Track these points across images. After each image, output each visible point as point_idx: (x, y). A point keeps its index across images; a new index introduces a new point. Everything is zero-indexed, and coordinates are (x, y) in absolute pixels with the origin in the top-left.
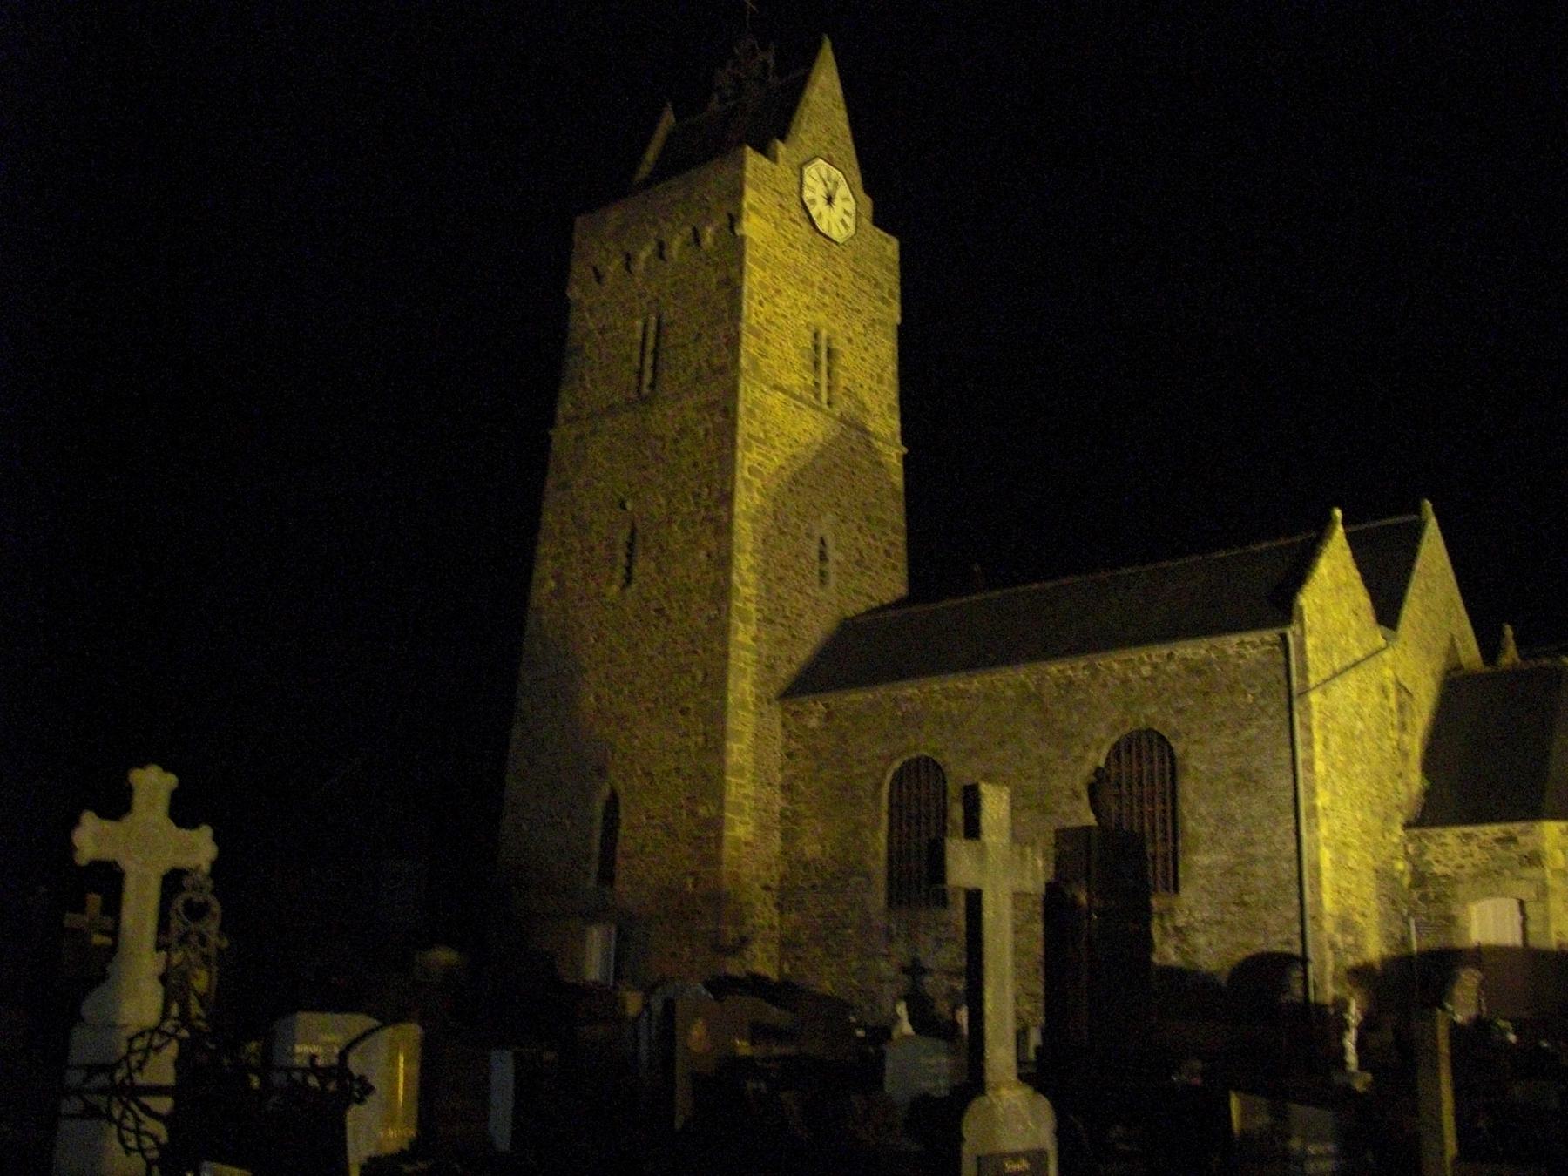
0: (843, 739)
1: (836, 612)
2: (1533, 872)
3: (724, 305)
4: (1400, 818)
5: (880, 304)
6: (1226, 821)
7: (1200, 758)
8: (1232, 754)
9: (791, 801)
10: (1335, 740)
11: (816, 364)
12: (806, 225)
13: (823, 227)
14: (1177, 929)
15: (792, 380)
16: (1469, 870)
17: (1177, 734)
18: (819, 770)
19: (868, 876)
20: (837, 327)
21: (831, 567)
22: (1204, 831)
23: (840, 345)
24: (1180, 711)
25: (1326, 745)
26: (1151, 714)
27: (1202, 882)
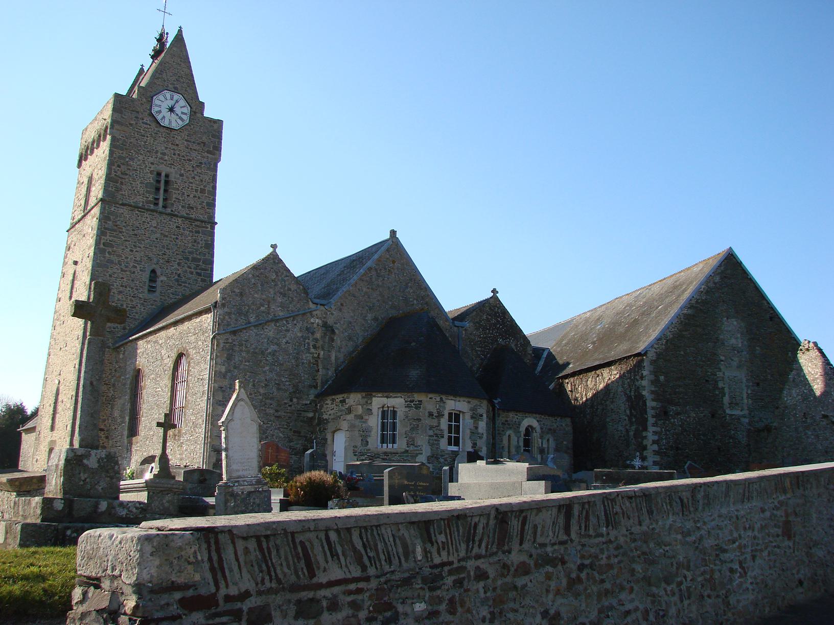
4: (313, 393)
11: (158, 189)
12: (154, 125)
15: (140, 200)
21: (159, 284)
23: (172, 178)
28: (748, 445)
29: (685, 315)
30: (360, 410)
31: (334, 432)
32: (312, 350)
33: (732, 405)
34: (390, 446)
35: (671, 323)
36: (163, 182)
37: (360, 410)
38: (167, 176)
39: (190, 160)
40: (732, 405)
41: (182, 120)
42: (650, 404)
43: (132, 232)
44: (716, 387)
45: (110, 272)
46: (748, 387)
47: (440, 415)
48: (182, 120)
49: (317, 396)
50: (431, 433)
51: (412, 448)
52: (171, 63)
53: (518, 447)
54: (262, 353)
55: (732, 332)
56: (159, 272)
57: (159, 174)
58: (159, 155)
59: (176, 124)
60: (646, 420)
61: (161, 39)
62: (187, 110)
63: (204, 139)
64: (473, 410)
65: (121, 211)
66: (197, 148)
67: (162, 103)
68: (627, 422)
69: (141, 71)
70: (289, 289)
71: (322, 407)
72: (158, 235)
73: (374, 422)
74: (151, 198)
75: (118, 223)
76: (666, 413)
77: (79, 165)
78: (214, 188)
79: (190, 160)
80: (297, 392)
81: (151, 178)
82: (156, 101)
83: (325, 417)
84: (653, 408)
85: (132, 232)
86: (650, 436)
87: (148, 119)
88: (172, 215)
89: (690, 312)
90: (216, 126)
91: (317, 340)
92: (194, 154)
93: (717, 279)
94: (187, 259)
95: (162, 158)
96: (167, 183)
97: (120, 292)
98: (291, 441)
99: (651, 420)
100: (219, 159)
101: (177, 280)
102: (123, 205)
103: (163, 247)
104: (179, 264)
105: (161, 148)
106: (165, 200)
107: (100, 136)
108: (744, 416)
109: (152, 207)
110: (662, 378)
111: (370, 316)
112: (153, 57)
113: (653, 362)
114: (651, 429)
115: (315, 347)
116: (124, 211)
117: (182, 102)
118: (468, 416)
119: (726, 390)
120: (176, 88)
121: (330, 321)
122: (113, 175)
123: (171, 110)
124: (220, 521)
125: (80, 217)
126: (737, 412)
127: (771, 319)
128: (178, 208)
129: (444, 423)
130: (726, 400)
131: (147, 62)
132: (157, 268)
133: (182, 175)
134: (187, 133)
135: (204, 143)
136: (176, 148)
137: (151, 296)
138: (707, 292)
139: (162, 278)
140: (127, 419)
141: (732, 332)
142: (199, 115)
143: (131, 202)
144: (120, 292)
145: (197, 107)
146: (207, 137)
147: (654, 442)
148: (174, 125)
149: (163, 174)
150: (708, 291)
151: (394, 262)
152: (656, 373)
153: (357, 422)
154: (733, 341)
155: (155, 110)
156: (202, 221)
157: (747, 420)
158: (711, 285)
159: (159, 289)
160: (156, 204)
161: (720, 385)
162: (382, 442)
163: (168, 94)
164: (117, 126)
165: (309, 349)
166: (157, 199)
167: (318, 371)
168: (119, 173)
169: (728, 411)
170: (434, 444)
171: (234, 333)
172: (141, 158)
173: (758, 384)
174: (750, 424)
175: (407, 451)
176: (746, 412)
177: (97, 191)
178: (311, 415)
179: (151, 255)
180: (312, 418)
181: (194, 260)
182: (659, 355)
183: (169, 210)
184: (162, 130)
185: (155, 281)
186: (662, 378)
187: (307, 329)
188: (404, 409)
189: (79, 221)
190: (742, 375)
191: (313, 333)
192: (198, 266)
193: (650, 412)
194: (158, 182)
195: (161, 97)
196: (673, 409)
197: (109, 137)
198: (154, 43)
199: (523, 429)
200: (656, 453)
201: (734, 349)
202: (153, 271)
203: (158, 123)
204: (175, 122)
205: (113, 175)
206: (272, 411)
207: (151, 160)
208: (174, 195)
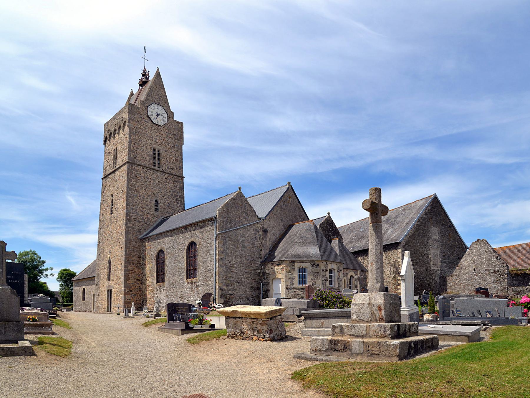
11: (155, 158)
12: (150, 122)
15: (146, 163)
20: (161, 148)
21: (159, 207)
23: (161, 152)
28: (440, 283)
29: (417, 225)
31: (273, 280)
32: (259, 240)
33: (434, 265)
34: (304, 285)
35: (411, 228)
36: (157, 154)
38: (158, 151)
40: (434, 265)
41: (164, 121)
45: (136, 201)
46: (440, 257)
47: (326, 271)
48: (164, 121)
49: (262, 262)
50: (323, 279)
52: (153, 88)
53: (348, 285)
54: (238, 241)
55: (435, 233)
56: (159, 201)
57: (154, 150)
58: (154, 140)
59: (161, 123)
61: (145, 74)
62: (165, 115)
63: (175, 132)
64: (338, 268)
65: (138, 168)
66: (172, 137)
67: (154, 110)
69: (132, 94)
70: (248, 210)
71: (264, 268)
72: (157, 182)
73: (296, 275)
74: (152, 162)
77: (105, 144)
78: (182, 159)
80: (253, 262)
81: (151, 152)
82: (150, 109)
83: (267, 272)
88: (163, 172)
89: (419, 223)
90: (180, 125)
91: (260, 235)
92: (171, 140)
93: (429, 208)
95: (155, 141)
96: (159, 154)
97: (141, 211)
98: (252, 284)
103: (160, 188)
104: (168, 198)
105: (154, 135)
106: (159, 164)
107: (120, 127)
109: (153, 167)
111: (281, 224)
112: (140, 85)
115: (260, 239)
116: (140, 168)
117: (163, 111)
118: (336, 271)
119: (432, 259)
121: (265, 226)
122: (132, 149)
124: (38, 323)
125: (111, 171)
126: (435, 269)
128: (165, 168)
129: (328, 274)
130: (432, 263)
131: (136, 89)
133: (166, 151)
134: (166, 128)
137: (156, 213)
139: (161, 204)
140: (155, 274)
141: (435, 233)
142: (171, 119)
144: (141, 211)
145: (170, 114)
146: (176, 131)
148: (160, 124)
149: (157, 150)
150: (426, 214)
151: (290, 198)
154: (435, 237)
155: (150, 114)
156: (177, 176)
157: (439, 272)
158: (427, 211)
159: (160, 210)
160: (155, 166)
161: (430, 256)
162: (300, 284)
163: (155, 105)
164: (131, 122)
165: (257, 240)
167: (261, 250)
168: (135, 148)
169: (432, 268)
170: (324, 284)
172: (145, 140)
173: (444, 256)
177: (123, 157)
178: (259, 271)
180: (260, 273)
181: (175, 196)
182: (406, 243)
183: (161, 170)
184: (154, 125)
185: (157, 206)
187: (256, 230)
188: (310, 268)
189: (110, 174)
190: (438, 252)
191: (258, 232)
194: (155, 154)
195: (152, 106)
197: (127, 129)
198: (140, 77)
199: (349, 277)
202: (156, 201)
203: (152, 121)
204: (161, 121)
205: (132, 149)
206: (244, 270)
207: (151, 142)
208: (163, 162)
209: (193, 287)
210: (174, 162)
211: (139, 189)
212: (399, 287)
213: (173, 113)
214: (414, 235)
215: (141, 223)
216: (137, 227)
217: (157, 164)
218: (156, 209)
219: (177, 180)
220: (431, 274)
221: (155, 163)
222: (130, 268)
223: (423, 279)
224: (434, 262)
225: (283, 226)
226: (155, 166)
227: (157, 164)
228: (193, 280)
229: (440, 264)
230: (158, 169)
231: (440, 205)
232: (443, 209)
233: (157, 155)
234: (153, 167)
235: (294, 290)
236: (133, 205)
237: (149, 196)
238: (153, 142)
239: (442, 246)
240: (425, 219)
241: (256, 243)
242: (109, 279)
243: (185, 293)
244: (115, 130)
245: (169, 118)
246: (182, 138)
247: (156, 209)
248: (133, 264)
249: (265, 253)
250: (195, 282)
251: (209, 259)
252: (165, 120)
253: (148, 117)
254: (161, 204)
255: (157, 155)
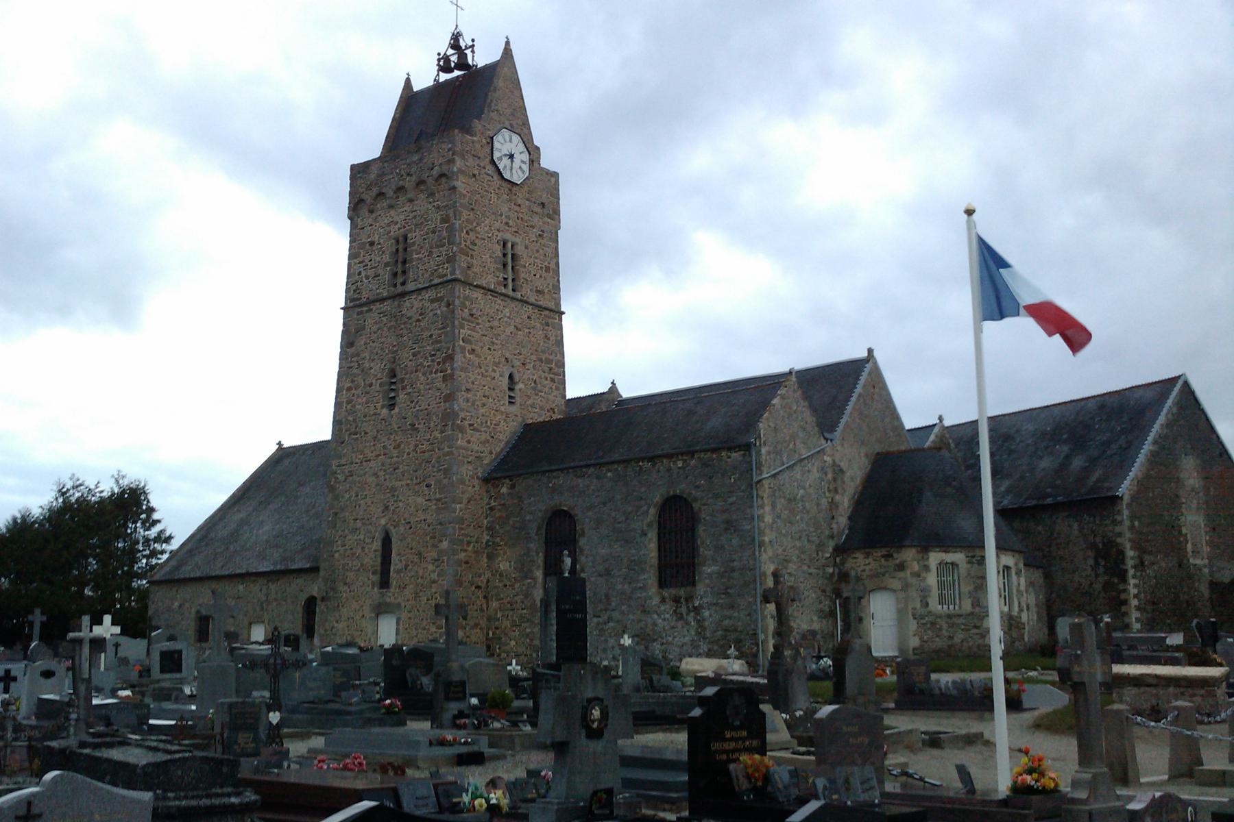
0: (520, 499)
1: (520, 419)
2: (901, 574)
3: (445, 234)
4: (831, 545)
5: (546, 219)
6: (719, 548)
7: (709, 512)
8: (724, 511)
9: (492, 536)
10: (781, 503)
11: (505, 265)
12: (496, 177)
13: (507, 175)
14: (695, 608)
15: (490, 280)
16: (867, 573)
17: (695, 500)
18: (508, 517)
19: (534, 579)
20: (518, 240)
21: (516, 394)
22: (709, 553)
23: (520, 250)
24: (697, 487)
25: (774, 506)
26: (681, 488)
27: (707, 581)
30: (916, 567)
33: (1196, 553)
37: (916, 567)
39: (533, 227)
42: (1130, 553)
43: (488, 325)
44: (1180, 532)
51: (977, 609)
56: (517, 378)
59: (518, 178)
60: (1126, 571)
62: (526, 157)
64: (1016, 564)
68: (1089, 571)
75: (474, 311)
76: (1142, 563)
79: (533, 227)
80: (820, 546)
84: (1132, 558)
85: (488, 325)
86: (1132, 586)
87: (490, 169)
90: (553, 180)
92: (536, 218)
94: (541, 360)
99: (1131, 572)
100: (557, 227)
101: (534, 389)
102: (477, 286)
105: (504, 209)
108: (1205, 566)
110: (1136, 523)
111: (863, 451)
113: (1129, 505)
114: (1132, 581)
115: (829, 491)
116: (478, 294)
120: (512, 125)
123: (511, 156)
126: (1198, 562)
127: (1221, 455)
128: (527, 292)
130: (1189, 547)
132: (515, 371)
135: (543, 204)
136: (517, 208)
137: (513, 409)
138: (1167, 425)
141: (1190, 472)
142: (536, 164)
143: (483, 283)
145: (533, 152)
147: (1136, 596)
152: (1132, 517)
153: (914, 581)
154: (1191, 482)
155: (496, 155)
157: (1206, 570)
159: (518, 400)
161: (1184, 531)
166: (505, 279)
169: (1191, 561)
171: (774, 476)
174: (1211, 572)
175: (972, 613)
176: (1206, 561)
178: (831, 570)
179: (507, 355)
184: (504, 184)
186: (1136, 523)
192: (551, 369)
193: (1130, 563)
194: (505, 255)
196: (1148, 559)
200: (1138, 608)
201: (1193, 490)
202: (511, 377)
203: (500, 173)
204: (517, 172)
207: (497, 225)
209: (684, 610)
210: (544, 274)
211: (477, 348)
212: (1124, 609)
213: (538, 149)
214: (1147, 477)
215: (484, 437)
216: (476, 448)
217: (510, 280)
218: (510, 397)
219: (550, 321)
220: (1190, 577)
221: (505, 279)
222: (462, 555)
223: (1175, 587)
224: (1194, 545)
225: (867, 455)
226: (505, 286)
227: (510, 280)
228: (682, 592)
229: (1206, 549)
230: (511, 293)
231: (1197, 402)
232: (1203, 411)
233: (509, 259)
234: (504, 291)
235: (931, 619)
236: (468, 390)
237: (497, 364)
238: (503, 227)
239: (1207, 503)
240: (1166, 436)
241: (824, 501)
242: (385, 583)
243: (655, 625)
244: (400, 189)
245: (532, 162)
246: (557, 212)
247: (510, 397)
248: (469, 543)
249: (842, 526)
250: (689, 599)
251: (735, 542)
252: (526, 167)
253: (493, 162)
254: (521, 386)
255: (509, 259)
